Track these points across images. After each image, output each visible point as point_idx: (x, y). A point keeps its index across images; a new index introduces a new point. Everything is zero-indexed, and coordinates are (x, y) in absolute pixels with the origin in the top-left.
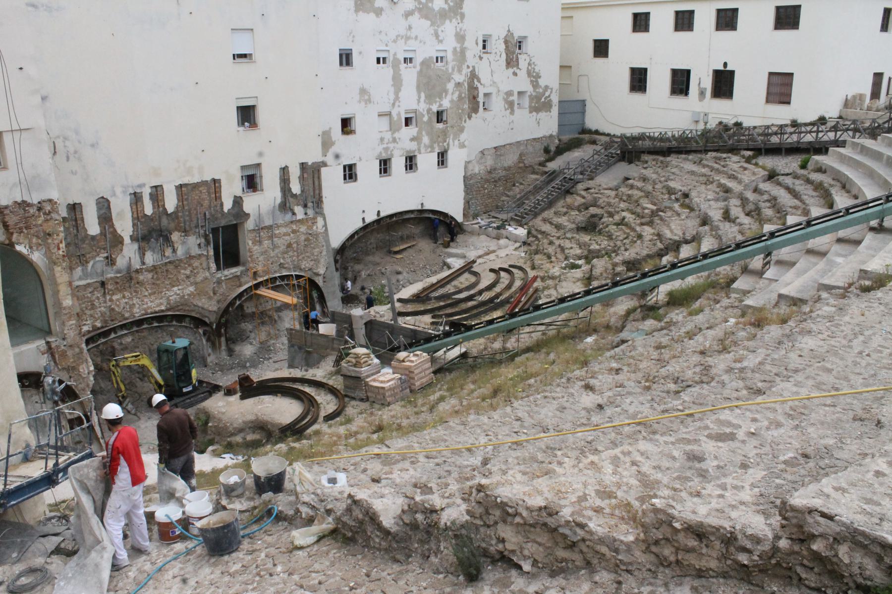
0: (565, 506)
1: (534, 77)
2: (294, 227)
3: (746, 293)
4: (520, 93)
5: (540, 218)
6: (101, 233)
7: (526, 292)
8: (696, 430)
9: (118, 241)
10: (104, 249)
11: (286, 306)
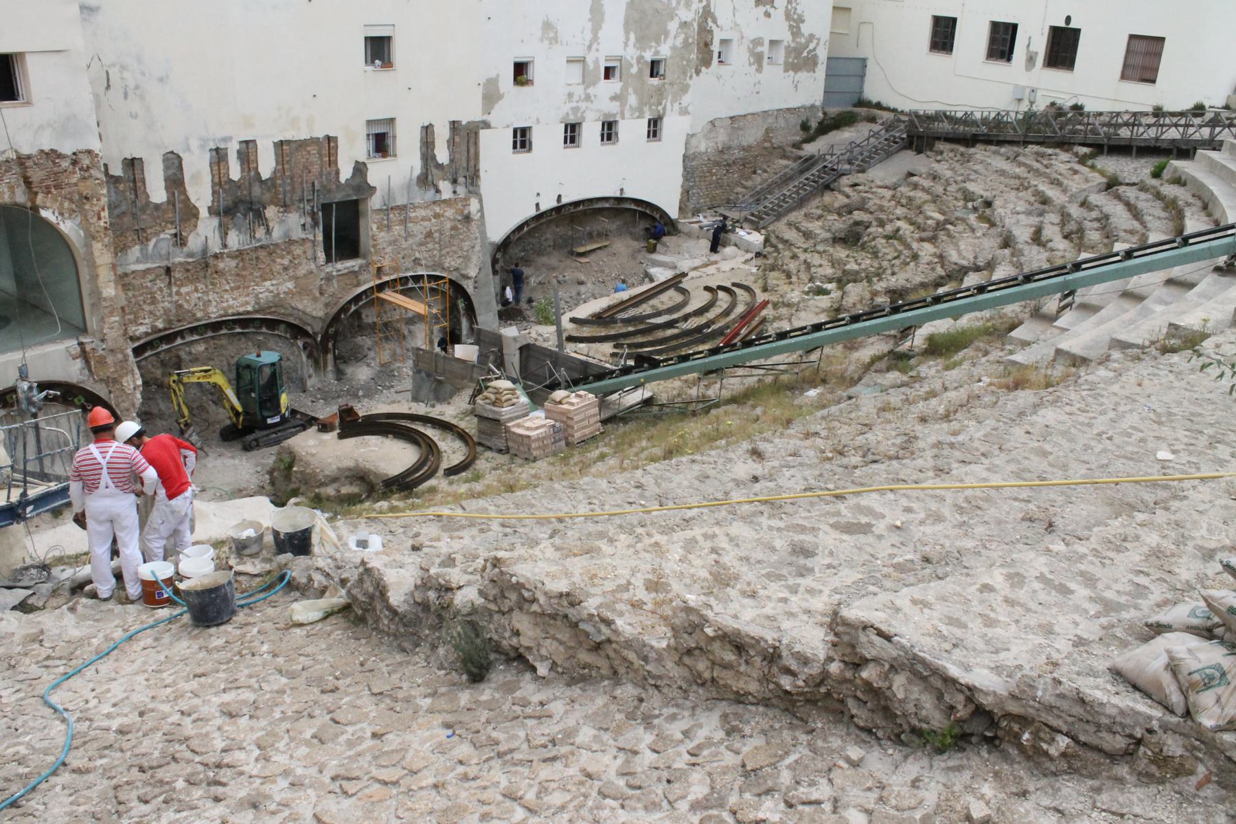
0: (594, 595)
1: (795, 21)
2: (437, 209)
3: (1025, 344)
4: (773, 43)
5: (784, 220)
6: (169, 202)
7: (749, 322)
8: (821, 515)
9: (191, 214)
10: (172, 223)
11: (419, 318)
